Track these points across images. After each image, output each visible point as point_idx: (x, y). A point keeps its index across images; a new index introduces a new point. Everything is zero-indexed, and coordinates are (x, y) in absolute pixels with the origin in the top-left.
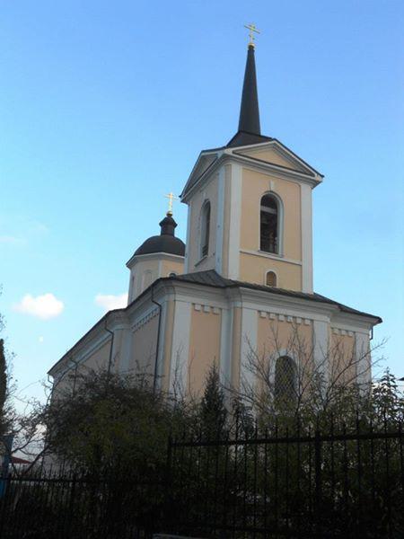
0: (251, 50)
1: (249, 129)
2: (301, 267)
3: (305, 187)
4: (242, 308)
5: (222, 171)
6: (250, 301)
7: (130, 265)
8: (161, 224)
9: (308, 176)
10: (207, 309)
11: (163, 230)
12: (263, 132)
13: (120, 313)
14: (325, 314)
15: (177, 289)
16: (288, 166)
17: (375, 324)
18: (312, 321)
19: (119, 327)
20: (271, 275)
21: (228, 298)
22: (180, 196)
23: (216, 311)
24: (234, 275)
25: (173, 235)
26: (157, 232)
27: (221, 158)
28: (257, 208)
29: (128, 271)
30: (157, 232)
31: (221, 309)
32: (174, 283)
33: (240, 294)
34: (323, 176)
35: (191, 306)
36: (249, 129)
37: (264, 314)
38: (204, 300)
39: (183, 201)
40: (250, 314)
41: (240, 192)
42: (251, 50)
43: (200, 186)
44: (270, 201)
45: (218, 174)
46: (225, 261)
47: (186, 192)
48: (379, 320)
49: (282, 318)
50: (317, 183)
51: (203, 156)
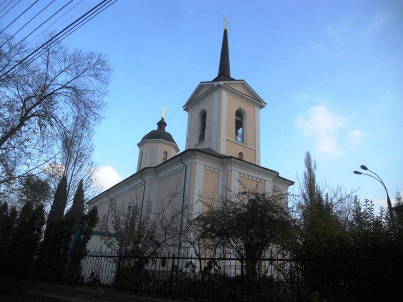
0: (226, 32)
1: (224, 72)
2: (255, 151)
3: (257, 108)
4: (231, 170)
5: (216, 94)
6: (235, 167)
7: (139, 145)
8: (158, 124)
9: (259, 103)
10: (212, 169)
11: (158, 127)
12: (232, 76)
13: (152, 169)
14: (270, 177)
15: (197, 156)
16: (246, 94)
17: (290, 185)
18: (265, 181)
19: (150, 177)
20: (241, 154)
21: (223, 165)
22: (183, 107)
23: (217, 171)
24: (223, 151)
25: (164, 130)
26: (156, 128)
27: (216, 86)
28: (233, 117)
29: (138, 149)
30: (156, 128)
31: (219, 170)
32: (196, 153)
33: (231, 162)
34: (266, 104)
35: (203, 166)
36: (224, 72)
37: (242, 175)
38: (213, 164)
39: (185, 110)
40: (235, 173)
41: (225, 105)
42: (226, 32)
43: (193, 105)
44: (239, 114)
45: (213, 96)
46: (218, 143)
47: (188, 105)
48: (293, 183)
49: (250, 178)
50: (262, 107)
51: (201, 85)
